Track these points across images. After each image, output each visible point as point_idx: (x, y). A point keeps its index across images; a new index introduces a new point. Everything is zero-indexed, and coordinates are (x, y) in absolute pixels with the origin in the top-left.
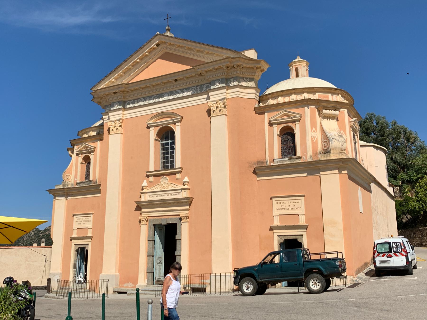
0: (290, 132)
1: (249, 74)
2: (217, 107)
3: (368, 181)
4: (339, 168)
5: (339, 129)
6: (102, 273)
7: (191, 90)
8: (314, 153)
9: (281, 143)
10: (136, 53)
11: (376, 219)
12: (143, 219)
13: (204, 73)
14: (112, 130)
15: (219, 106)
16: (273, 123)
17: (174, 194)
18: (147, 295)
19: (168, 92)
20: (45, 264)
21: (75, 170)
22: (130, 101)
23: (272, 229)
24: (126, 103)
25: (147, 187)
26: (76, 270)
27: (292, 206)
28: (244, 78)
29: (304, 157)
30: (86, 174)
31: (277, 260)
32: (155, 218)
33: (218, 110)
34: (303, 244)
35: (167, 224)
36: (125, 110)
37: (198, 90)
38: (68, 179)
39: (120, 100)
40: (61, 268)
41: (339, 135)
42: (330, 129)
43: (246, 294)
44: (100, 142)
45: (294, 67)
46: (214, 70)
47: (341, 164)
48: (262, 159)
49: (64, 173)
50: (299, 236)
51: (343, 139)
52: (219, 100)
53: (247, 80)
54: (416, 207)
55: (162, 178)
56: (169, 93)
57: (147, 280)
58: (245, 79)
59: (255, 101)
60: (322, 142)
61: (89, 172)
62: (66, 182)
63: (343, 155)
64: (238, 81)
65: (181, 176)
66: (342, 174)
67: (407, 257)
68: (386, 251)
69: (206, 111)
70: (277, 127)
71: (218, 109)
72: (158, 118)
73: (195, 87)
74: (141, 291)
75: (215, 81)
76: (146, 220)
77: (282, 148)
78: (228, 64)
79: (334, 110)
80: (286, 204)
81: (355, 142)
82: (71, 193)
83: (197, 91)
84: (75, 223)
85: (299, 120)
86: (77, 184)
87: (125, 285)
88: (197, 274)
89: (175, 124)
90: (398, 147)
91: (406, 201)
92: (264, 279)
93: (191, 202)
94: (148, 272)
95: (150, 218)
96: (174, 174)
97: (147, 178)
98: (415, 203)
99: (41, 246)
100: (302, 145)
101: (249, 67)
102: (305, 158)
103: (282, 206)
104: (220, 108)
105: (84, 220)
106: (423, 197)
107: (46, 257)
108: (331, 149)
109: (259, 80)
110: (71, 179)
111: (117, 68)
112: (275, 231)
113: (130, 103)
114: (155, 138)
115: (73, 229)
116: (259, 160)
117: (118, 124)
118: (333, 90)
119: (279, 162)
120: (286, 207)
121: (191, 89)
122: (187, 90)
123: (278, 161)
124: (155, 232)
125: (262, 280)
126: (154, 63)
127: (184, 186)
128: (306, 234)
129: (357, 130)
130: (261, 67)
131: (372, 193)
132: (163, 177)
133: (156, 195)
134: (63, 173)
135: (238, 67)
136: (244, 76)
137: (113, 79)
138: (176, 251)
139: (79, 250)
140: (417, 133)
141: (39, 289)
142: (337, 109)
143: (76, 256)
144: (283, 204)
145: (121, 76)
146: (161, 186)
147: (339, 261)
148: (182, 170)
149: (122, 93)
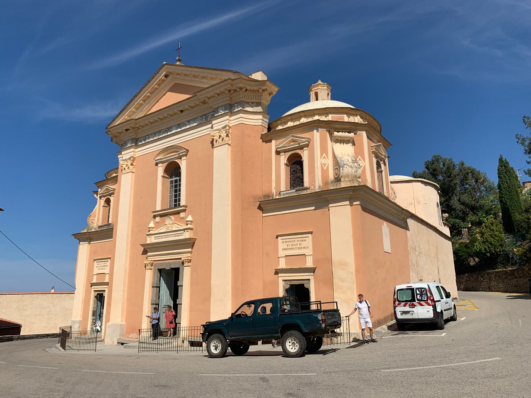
1: (255, 98)
2: (220, 136)
3: (401, 217)
4: (350, 199)
5: (354, 154)
8: (323, 183)
9: (289, 173)
10: (145, 86)
11: (416, 261)
13: (207, 100)
15: (221, 135)
16: (280, 151)
17: (177, 235)
23: (277, 273)
25: (153, 228)
27: (299, 245)
28: (249, 103)
31: (287, 307)
33: (221, 139)
34: (310, 290)
35: (171, 268)
36: (137, 147)
37: (204, 120)
38: (93, 223)
40: (81, 316)
41: (353, 161)
42: (342, 154)
43: (213, 355)
45: (314, 92)
46: (217, 96)
47: (351, 193)
48: (268, 192)
51: (357, 165)
52: (221, 128)
53: (253, 104)
54: (482, 249)
55: (167, 218)
56: (177, 126)
58: (251, 104)
59: (262, 128)
60: (333, 170)
62: (91, 226)
63: (355, 183)
64: (242, 106)
66: (354, 205)
67: (435, 307)
68: (408, 299)
70: (284, 155)
73: (200, 116)
75: (219, 107)
76: (151, 264)
77: (290, 178)
78: (229, 87)
79: (348, 132)
80: (293, 243)
81: (381, 171)
82: (93, 238)
83: (203, 121)
85: (307, 146)
86: (100, 227)
87: (131, 336)
89: (181, 158)
90: (466, 189)
91: (472, 243)
92: (234, 337)
93: (194, 243)
95: (155, 262)
96: (178, 213)
98: (480, 244)
101: (253, 90)
103: (288, 246)
104: (223, 137)
105: (103, 265)
106: (489, 238)
108: (341, 177)
109: (268, 106)
111: (129, 104)
112: (280, 275)
113: (142, 140)
114: (162, 175)
117: (129, 163)
118: (349, 110)
119: (285, 194)
120: (293, 247)
121: (197, 119)
125: (233, 338)
126: (164, 96)
129: (383, 157)
130: (267, 89)
131: (409, 231)
134: (88, 217)
135: (241, 90)
136: (249, 101)
137: (125, 116)
139: (98, 296)
140: (486, 173)
142: (351, 131)
145: (142, 104)
147: (322, 314)
148: (186, 209)
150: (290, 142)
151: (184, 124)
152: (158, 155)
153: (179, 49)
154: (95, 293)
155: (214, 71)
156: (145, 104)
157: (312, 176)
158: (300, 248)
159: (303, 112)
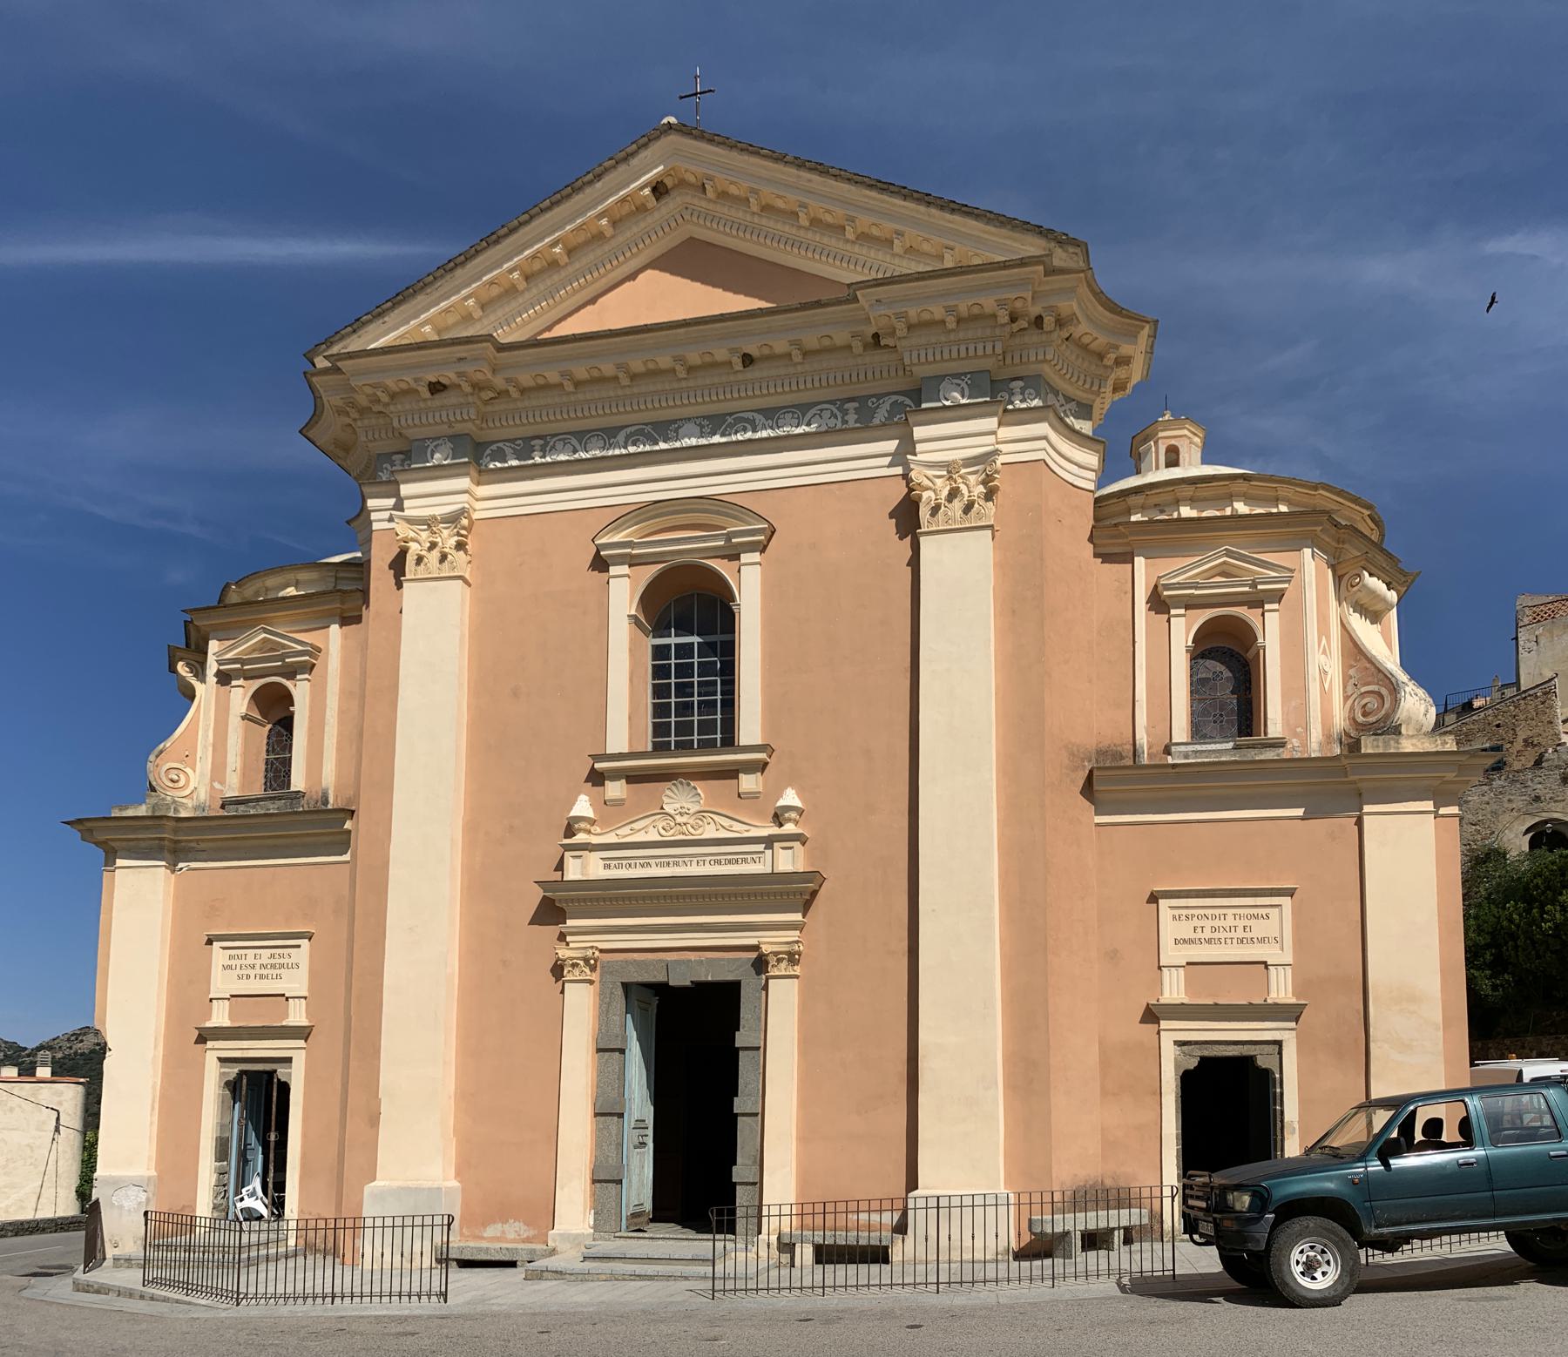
6: (374, 1180)
12: (575, 961)
14: (420, 560)
18: (624, 1280)
19: (697, 418)
20: (54, 1139)
21: (214, 746)
22: (507, 444)
23: (1152, 1015)
24: (488, 451)
25: (592, 822)
26: (229, 1164)
27: (1240, 929)
30: (266, 770)
32: (636, 956)
38: (176, 785)
45: (1163, 444)
48: (1118, 742)
49: (157, 757)
53: (1068, 407)
56: (705, 422)
57: (593, 1211)
61: (287, 763)
62: (169, 798)
69: (890, 514)
71: (956, 501)
74: (586, 1263)
80: (1217, 923)
82: (193, 845)
84: (217, 973)
85: (1278, 596)
87: (490, 1231)
93: (814, 894)
94: (600, 1181)
96: (730, 773)
97: (593, 786)
99: (34, 1076)
100: (1286, 696)
103: (1199, 930)
105: (265, 961)
107: (59, 1114)
110: (191, 788)
111: (451, 270)
112: (210, 1044)
113: (508, 451)
114: (633, 612)
115: (211, 1000)
116: (1105, 744)
117: (448, 539)
120: (1216, 935)
121: (813, 411)
122: (793, 413)
124: (629, 1016)
125: (1385, 1230)
127: (781, 825)
128: (1295, 1040)
132: (674, 784)
133: (638, 861)
138: (737, 1096)
139: (245, 1081)
141: (31, 1233)
143: (224, 1110)
145: (511, 291)
146: (664, 823)
149: (472, 394)
151: (747, 420)
152: (615, 524)
153: (696, 94)
154: (223, 1070)
155: (948, 216)
156: (527, 296)
157: (1293, 704)
158: (1245, 941)
159: (1245, 479)
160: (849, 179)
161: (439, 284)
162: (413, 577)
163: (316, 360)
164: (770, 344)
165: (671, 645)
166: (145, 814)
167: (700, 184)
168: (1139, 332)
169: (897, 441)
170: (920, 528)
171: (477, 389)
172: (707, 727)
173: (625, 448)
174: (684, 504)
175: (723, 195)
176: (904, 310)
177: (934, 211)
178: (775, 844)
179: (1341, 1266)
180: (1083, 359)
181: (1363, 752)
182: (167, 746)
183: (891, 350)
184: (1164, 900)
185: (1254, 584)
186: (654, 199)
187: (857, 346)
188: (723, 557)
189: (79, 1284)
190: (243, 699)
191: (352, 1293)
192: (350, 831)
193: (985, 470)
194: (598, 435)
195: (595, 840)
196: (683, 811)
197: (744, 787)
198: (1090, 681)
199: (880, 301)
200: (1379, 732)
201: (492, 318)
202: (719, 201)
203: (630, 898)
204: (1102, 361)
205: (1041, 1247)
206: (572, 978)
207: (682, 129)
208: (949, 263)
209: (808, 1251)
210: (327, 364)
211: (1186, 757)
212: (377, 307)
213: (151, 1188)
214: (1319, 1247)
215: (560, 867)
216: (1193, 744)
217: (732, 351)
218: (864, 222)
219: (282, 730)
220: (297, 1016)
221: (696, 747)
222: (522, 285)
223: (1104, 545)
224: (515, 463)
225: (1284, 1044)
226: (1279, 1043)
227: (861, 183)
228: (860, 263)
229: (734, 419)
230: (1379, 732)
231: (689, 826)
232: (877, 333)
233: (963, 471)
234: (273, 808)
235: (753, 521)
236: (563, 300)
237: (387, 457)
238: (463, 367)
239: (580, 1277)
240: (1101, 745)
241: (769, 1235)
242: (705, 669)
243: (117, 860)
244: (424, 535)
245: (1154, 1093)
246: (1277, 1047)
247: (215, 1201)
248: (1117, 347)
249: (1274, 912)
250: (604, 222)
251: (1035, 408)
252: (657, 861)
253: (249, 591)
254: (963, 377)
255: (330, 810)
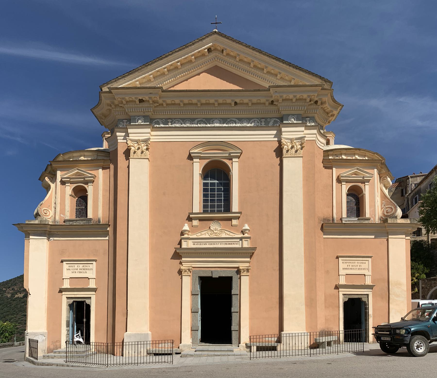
0: (353, 193)
7: (253, 121)
17: (229, 243)
19: (219, 118)
23: (337, 287)
24: (154, 122)
27: (359, 266)
29: (372, 220)
32: (202, 269)
39: (147, 114)
44: (102, 170)
49: (40, 206)
50: (364, 295)
56: (221, 120)
57: (191, 338)
62: (44, 219)
65: (239, 223)
69: (274, 151)
72: (204, 149)
73: (258, 118)
80: (353, 264)
84: (65, 271)
85: (368, 181)
88: (310, 333)
93: (253, 253)
94: (193, 330)
96: (230, 219)
97: (188, 221)
100: (370, 207)
102: (373, 221)
103: (349, 266)
105: (81, 267)
111: (147, 66)
112: (63, 293)
113: (160, 122)
116: (325, 217)
120: (353, 267)
122: (247, 120)
123: (347, 220)
126: (197, 76)
127: (244, 234)
128: (372, 294)
132: (214, 222)
133: (203, 243)
139: (75, 304)
144: (349, 264)
145: (163, 74)
146: (210, 233)
150: (352, 174)
151: (233, 121)
152: (196, 147)
155: (295, 70)
156: (168, 76)
157: (372, 209)
160: (268, 56)
161: (143, 69)
162: (133, 157)
163: (103, 89)
164: (243, 100)
165: (209, 183)
166: (37, 223)
167: (221, 50)
168: (338, 108)
169: (276, 131)
170: (130, 157)
171: (153, 103)
172: (219, 206)
173: (197, 124)
174: (217, 143)
175: (228, 55)
176: (283, 95)
177: (291, 68)
178: (243, 239)
179: (425, 347)
180: (324, 113)
181: (388, 222)
182: (43, 203)
183: (276, 106)
184: (340, 258)
185: (363, 178)
186: (208, 53)
187: (267, 103)
188: (227, 159)
189: (38, 363)
190: (70, 190)
191: (129, 363)
192: (109, 231)
193: (301, 141)
194: (189, 120)
195: (191, 237)
196: (216, 229)
197: (194, 224)
198: (322, 200)
199: (276, 92)
200: (391, 217)
201: (157, 81)
202: (227, 56)
203: (201, 253)
204: (328, 115)
205: (315, 346)
206: (185, 275)
207: (219, 34)
208: (292, 83)
209: (255, 348)
210: (108, 90)
211: (346, 221)
212: (124, 74)
213: (46, 336)
214: (420, 342)
215: (180, 243)
216: (347, 218)
217: (232, 100)
218: (270, 68)
219: (81, 200)
220: (92, 284)
221: (216, 212)
222: (167, 73)
223: (326, 164)
224: (162, 125)
225: (369, 295)
226: (368, 295)
227: (271, 57)
228: (267, 80)
229: (230, 120)
230: (391, 217)
231: (218, 233)
232: (273, 100)
233: (295, 141)
234: (82, 223)
235: (236, 149)
236: (178, 79)
237: (122, 120)
238: (150, 96)
239: (199, 356)
240: (324, 217)
241: (243, 344)
242: (219, 190)
243: (30, 236)
244: (136, 145)
245: (337, 307)
246: (367, 296)
247: (67, 339)
248: (332, 111)
249: (367, 262)
250: (193, 57)
251: (313, 126)
252: (209, 243)
253: (66, 157)
254: (295, 115)
255: (101, 224)
